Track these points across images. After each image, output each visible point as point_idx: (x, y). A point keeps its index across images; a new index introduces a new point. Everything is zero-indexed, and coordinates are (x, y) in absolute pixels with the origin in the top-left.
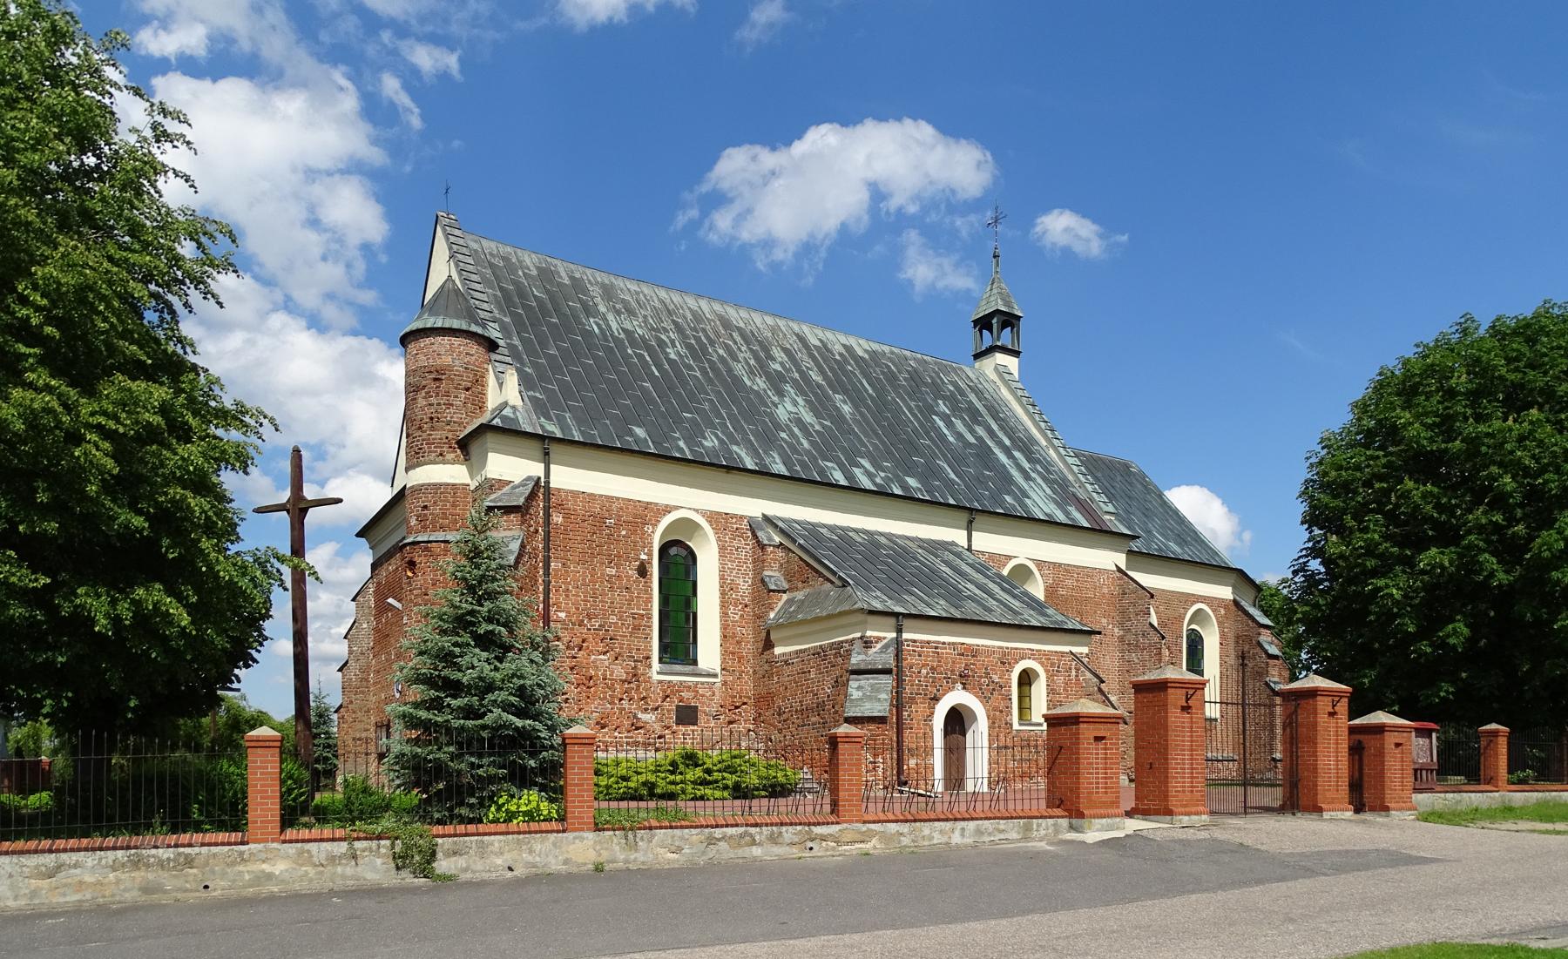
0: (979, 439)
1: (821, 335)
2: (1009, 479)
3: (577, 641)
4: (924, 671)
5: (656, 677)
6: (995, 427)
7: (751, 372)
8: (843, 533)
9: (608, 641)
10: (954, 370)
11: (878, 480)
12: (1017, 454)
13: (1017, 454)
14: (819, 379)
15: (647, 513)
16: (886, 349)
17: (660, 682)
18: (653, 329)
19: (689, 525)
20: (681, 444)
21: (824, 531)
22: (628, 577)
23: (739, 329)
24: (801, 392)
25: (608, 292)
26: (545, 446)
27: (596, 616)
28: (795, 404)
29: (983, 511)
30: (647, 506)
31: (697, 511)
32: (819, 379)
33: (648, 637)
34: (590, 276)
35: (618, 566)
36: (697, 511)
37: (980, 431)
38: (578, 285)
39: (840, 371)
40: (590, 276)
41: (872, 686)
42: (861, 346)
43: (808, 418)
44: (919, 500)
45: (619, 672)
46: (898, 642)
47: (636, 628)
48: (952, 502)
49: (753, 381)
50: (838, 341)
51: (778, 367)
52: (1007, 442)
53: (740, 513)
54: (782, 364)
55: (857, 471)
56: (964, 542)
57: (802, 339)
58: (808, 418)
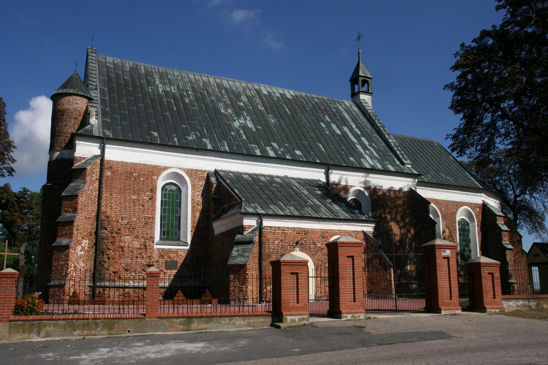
0: (344, 133)
1: (269, 90)
2: (355, 150)
3: (116, 229)
4: (276, 242)
5: (156, 247)
6: (354, 126)
7: (226, 107)
8: (255, 178)
9: (132, 229)
10: (339, 102)
11: (280, 152)
12: (363, 139)
13: (363, 139)
14: (263, 109)
15: (156, 170)
16: (303, 94)
17: (157, 249)
18: (181, 90)
19: (177, 176)
20: (176, 139)
21: (293, 181)
22: (143, 200)
23: (226, 89)
24: (249, 114)
25: (163, 76)
26: (103, 141)
27: (126, 218)
28: (245, 119)
29: (334, 165)
30: (155, 167)
31: (180, 169)
32: (263, 109)
33: (152, 228)
34: (156, 68)
35: (138, 194)
36: (180, 169)
37: (345, 129)
38: (148, 74)
39: (274, 105)
40: (156, 68)
41: (243, 249)
42: (289, 94)
43: (250, 125)
44: (301, 161)
45: (137, 244)
46: (260, 227)
47: (147, 223)
48: (318, 161)
49: (226, 110)
50: (277, 92)
51: (242, 104)
52: (359, 133)
53: (203, 169)
54: (244, 103)
55: (268, 148)
56: (324, 180)
57: (259, 92)
58: (250, 125)
